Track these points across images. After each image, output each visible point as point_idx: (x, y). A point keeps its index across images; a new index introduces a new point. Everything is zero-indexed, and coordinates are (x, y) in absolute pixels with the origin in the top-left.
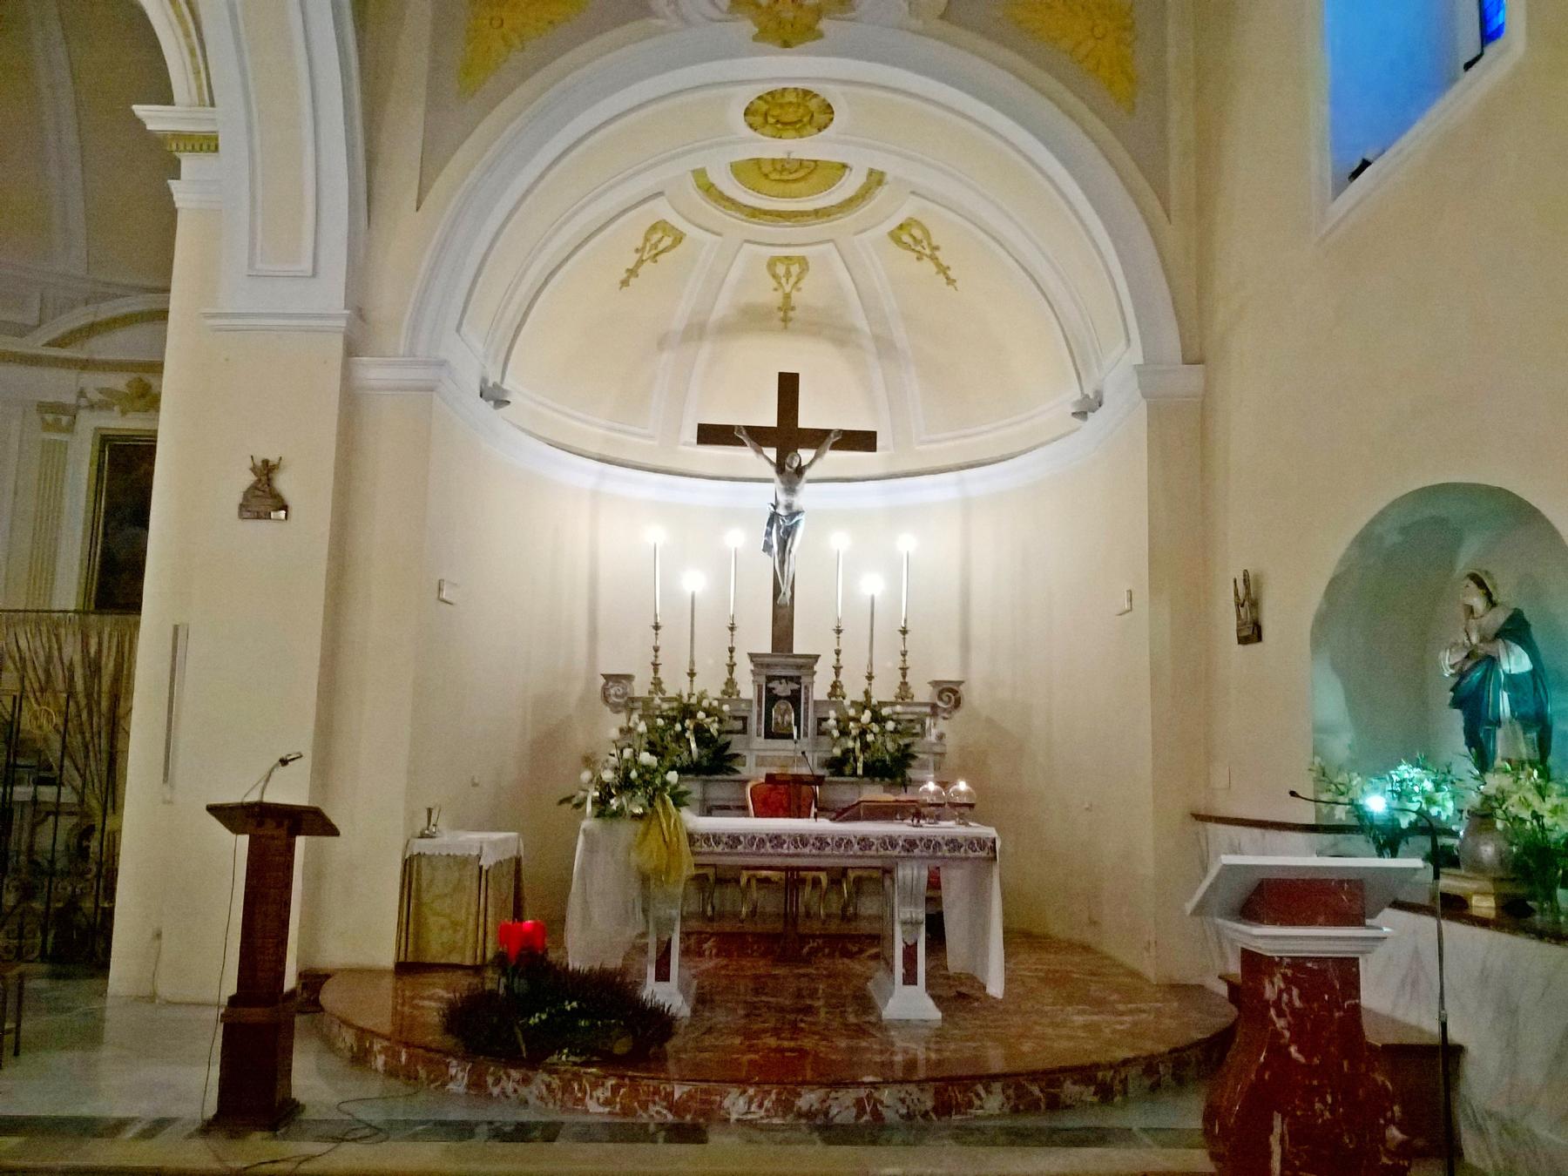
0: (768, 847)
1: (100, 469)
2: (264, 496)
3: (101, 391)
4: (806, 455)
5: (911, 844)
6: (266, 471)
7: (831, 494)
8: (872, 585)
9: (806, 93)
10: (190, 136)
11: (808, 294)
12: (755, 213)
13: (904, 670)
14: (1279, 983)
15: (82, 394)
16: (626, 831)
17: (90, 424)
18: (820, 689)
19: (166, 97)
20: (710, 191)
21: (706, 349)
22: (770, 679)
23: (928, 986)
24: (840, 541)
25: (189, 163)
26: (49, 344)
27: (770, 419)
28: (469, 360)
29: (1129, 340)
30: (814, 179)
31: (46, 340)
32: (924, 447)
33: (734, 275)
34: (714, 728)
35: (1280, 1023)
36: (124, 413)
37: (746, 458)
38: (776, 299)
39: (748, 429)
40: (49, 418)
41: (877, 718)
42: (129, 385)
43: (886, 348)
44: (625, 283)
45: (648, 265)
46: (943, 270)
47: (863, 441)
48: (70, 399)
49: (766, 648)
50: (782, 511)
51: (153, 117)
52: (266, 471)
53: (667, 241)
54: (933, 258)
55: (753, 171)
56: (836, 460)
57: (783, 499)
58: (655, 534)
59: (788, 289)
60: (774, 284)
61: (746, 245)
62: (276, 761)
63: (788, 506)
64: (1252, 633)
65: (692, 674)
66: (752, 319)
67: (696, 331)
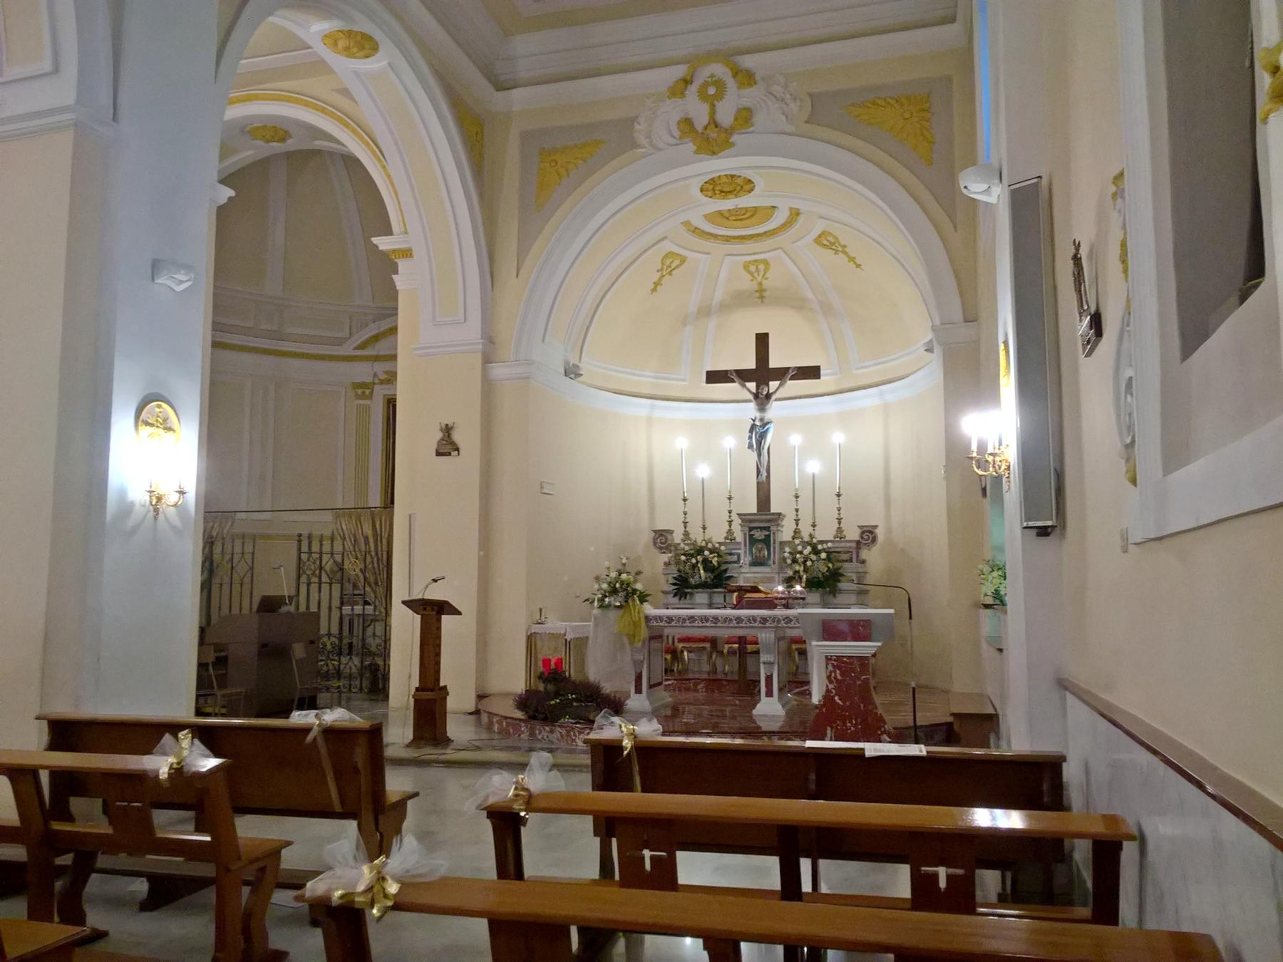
2: (447, 447)
3: (386, 373)
5: (764, 620)
6: (448, 430)
8: (814, 467)
9: (732, 176)
10: (399, 250)
11: (773, 280)
12: (728, 239)
13: (839, 520)
15: (375, 375)
16: (612, 615)
18: (786, 533)
19: (388, 231)
20: (696, 231)
21: (712, 323)
22: (751, 529)
23: (780, 698)
24: (796, 439)
25: (402, 265)
27: (751, 365)
28: (554, 354)
30: (754, 219)
33: (723, 275)
34: (715, 561)
37: (732, 389)
39: (736, 371)
40: (359, 391)
41: (816, 552)
43: (827, 310)
44: (654, 290)
45: (667, 277)
46: (852, 259)
47: (812, 372)
48: (369, 379)
49: (753, 509)
50: (758, 423)
51: (383, 243)
52: (448, 430)
53: (677, 262)
54: (845, 253)
56: (793, 386)
57: (758, 415)
58: (682, 443)
59: (759, 279)
62: (430, 580)
65: (704, 528)
66: (739, 300)
67: (705, 311)
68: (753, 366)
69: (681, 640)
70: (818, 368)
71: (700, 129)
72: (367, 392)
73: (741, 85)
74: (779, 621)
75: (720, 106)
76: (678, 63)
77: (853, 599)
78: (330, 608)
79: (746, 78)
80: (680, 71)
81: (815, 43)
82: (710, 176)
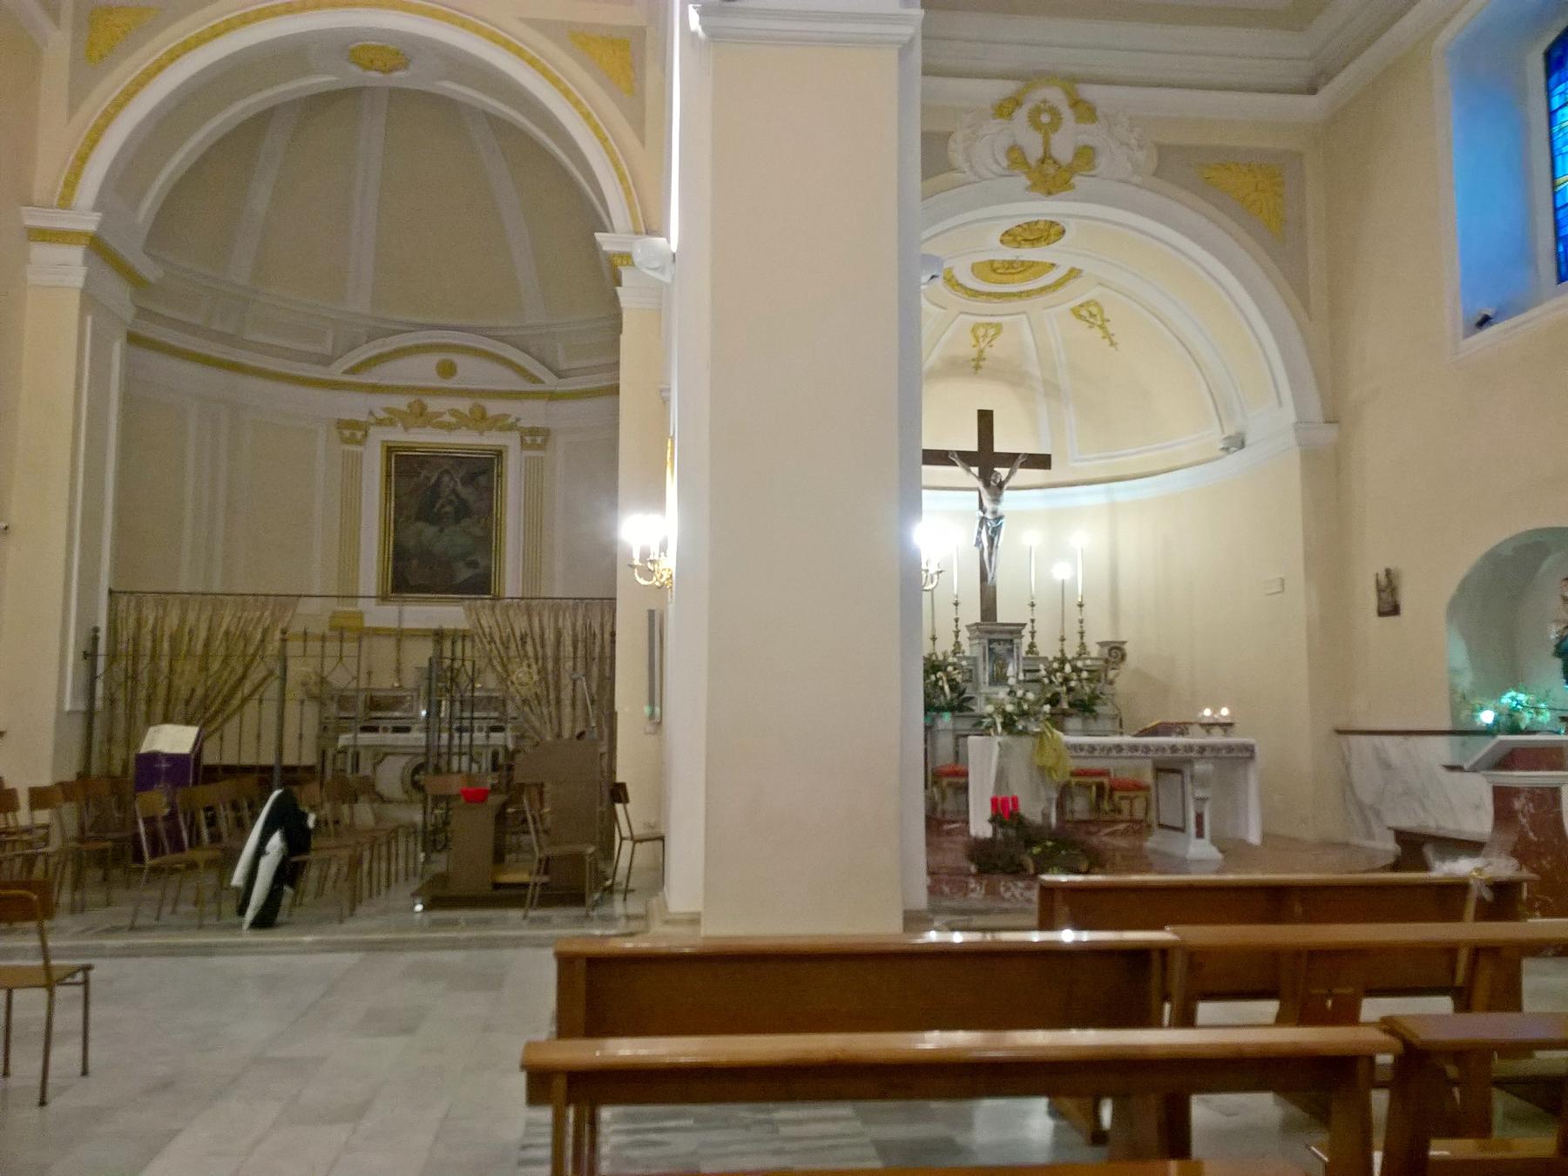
0: (1114, 753)
1: (388, 476)
3: (386, 410)
4: (1003, 472)
5: (1202, 749)
7: (1022, 499)
14: (1523, 800)
17: (380, 437)
22: (991, 641)
26: (345, 372)
29: (1280, 403)
31: (346, 367)
32: (1076, 464)
35: (1524, 821)
36: (406, 428)
37: (956, 474)
38: (974, 353)
39: (959, 453)
40: (347, 433)
42: (410, 406)
43: (1052, 390)
47: (1041, 461)
50: (989, 516)
54: (1102, 327)
55: (993, 269)
56: (1024, 475)
60: (973, 342)
61: (962, 316)
63: (994, 512)
64: (1390, 609)
65: (934, 639)
68: (996, 450)
69: (1073, 774)
70: (1048, 457)
71: (1033, 163)
72: (539, 440)
73: (1079, 118)
74: (1164, 749)
75: (1056, 139)
76: (1008, 78)
77: (1108, 725)
78: (110, 739)
79: (1085, 111)
80: (1010, 87)
81: (1173, 86)
82: (1021, 221)
